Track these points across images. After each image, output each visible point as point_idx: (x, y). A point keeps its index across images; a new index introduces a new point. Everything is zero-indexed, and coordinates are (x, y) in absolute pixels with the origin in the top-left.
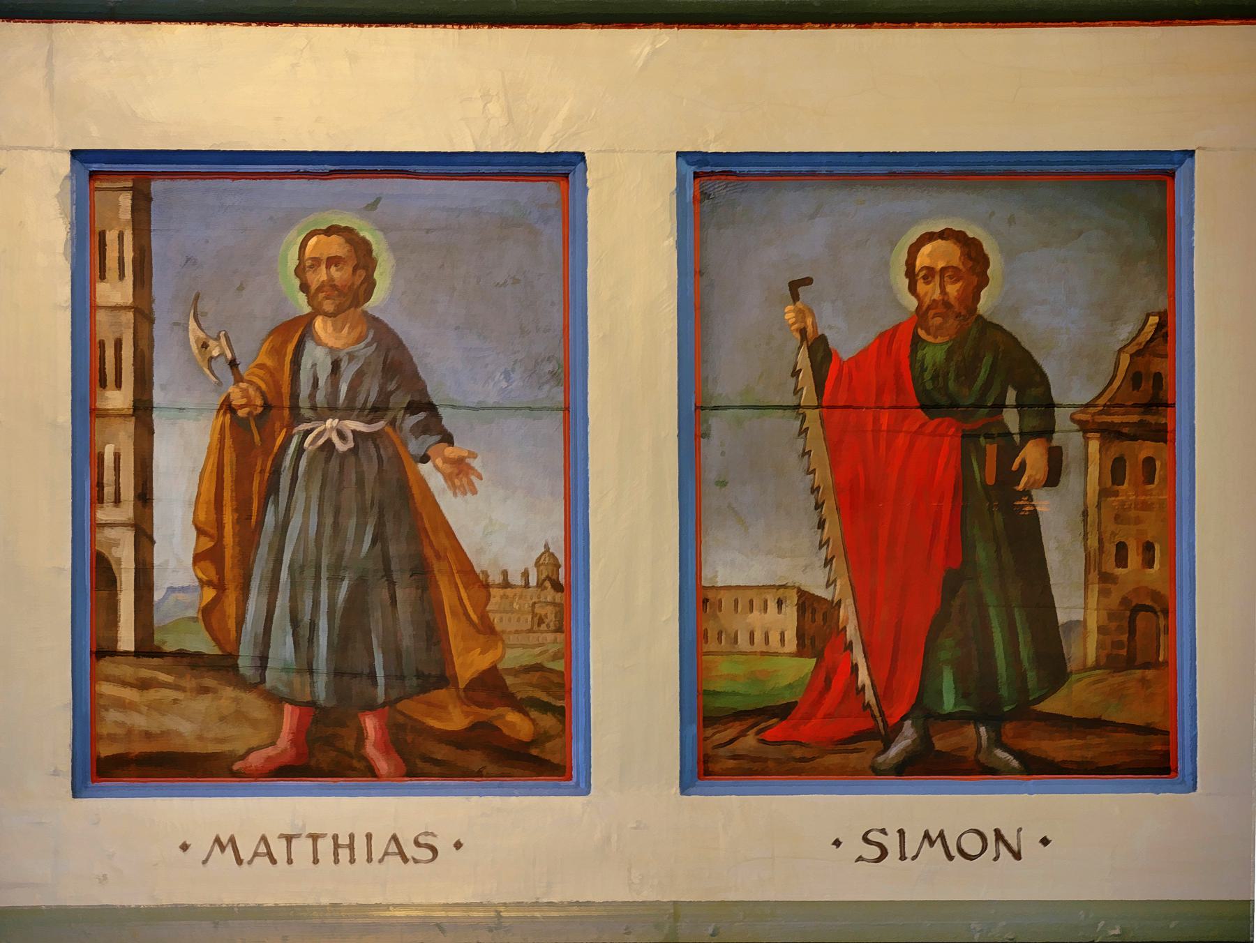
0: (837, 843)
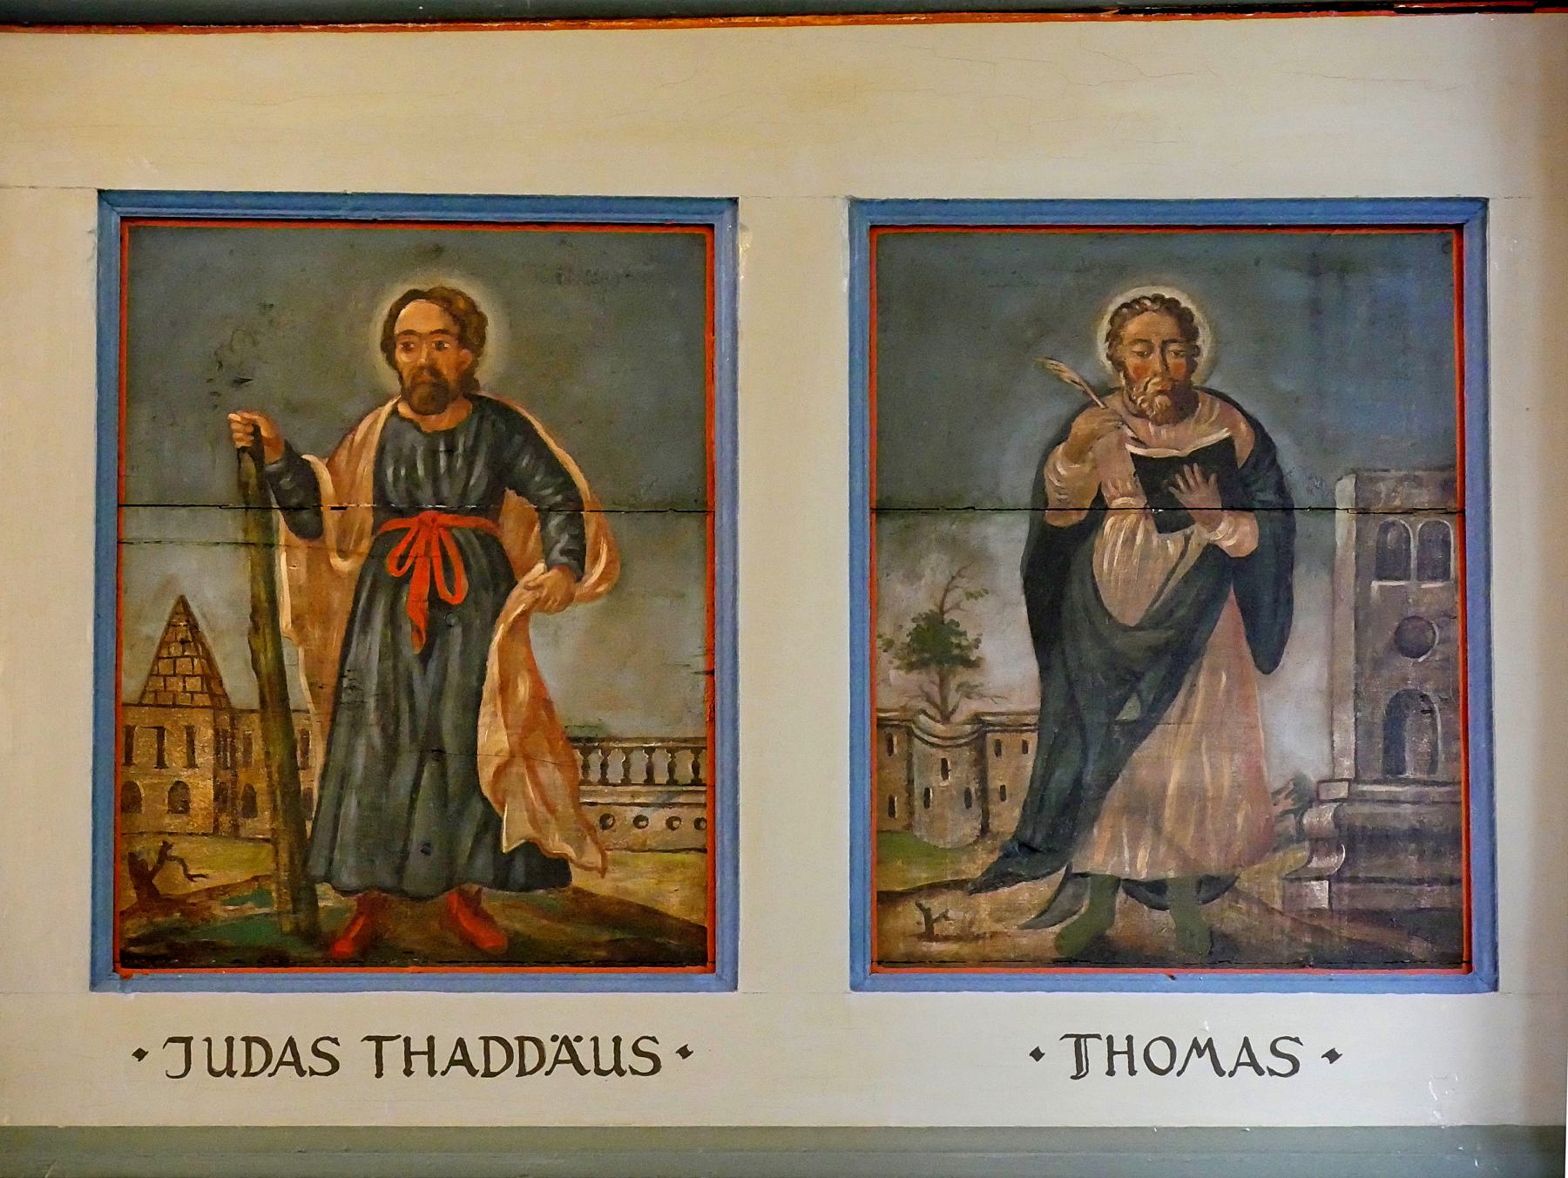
0: (1037, 1054)
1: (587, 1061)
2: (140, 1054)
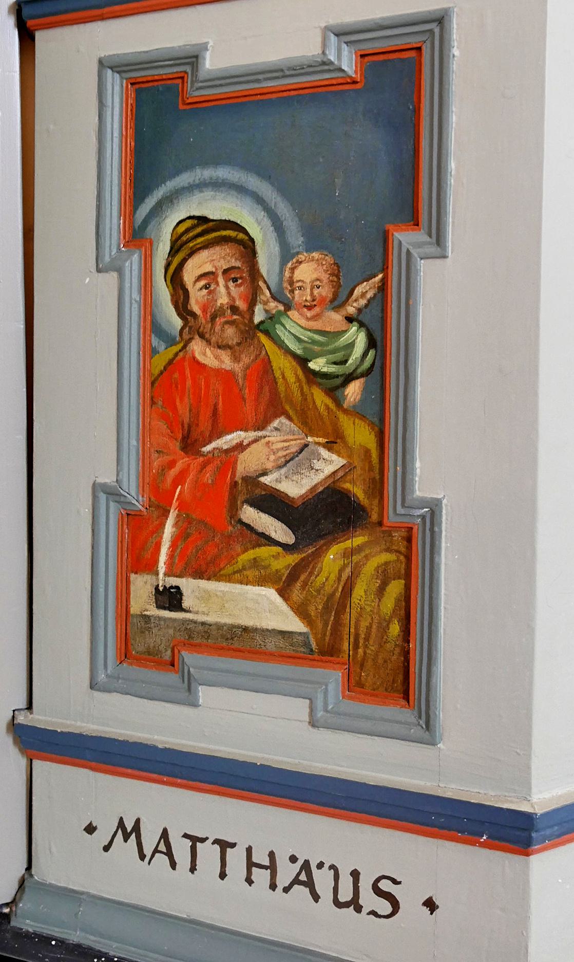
1: (326, 893)
2: (430, 905)
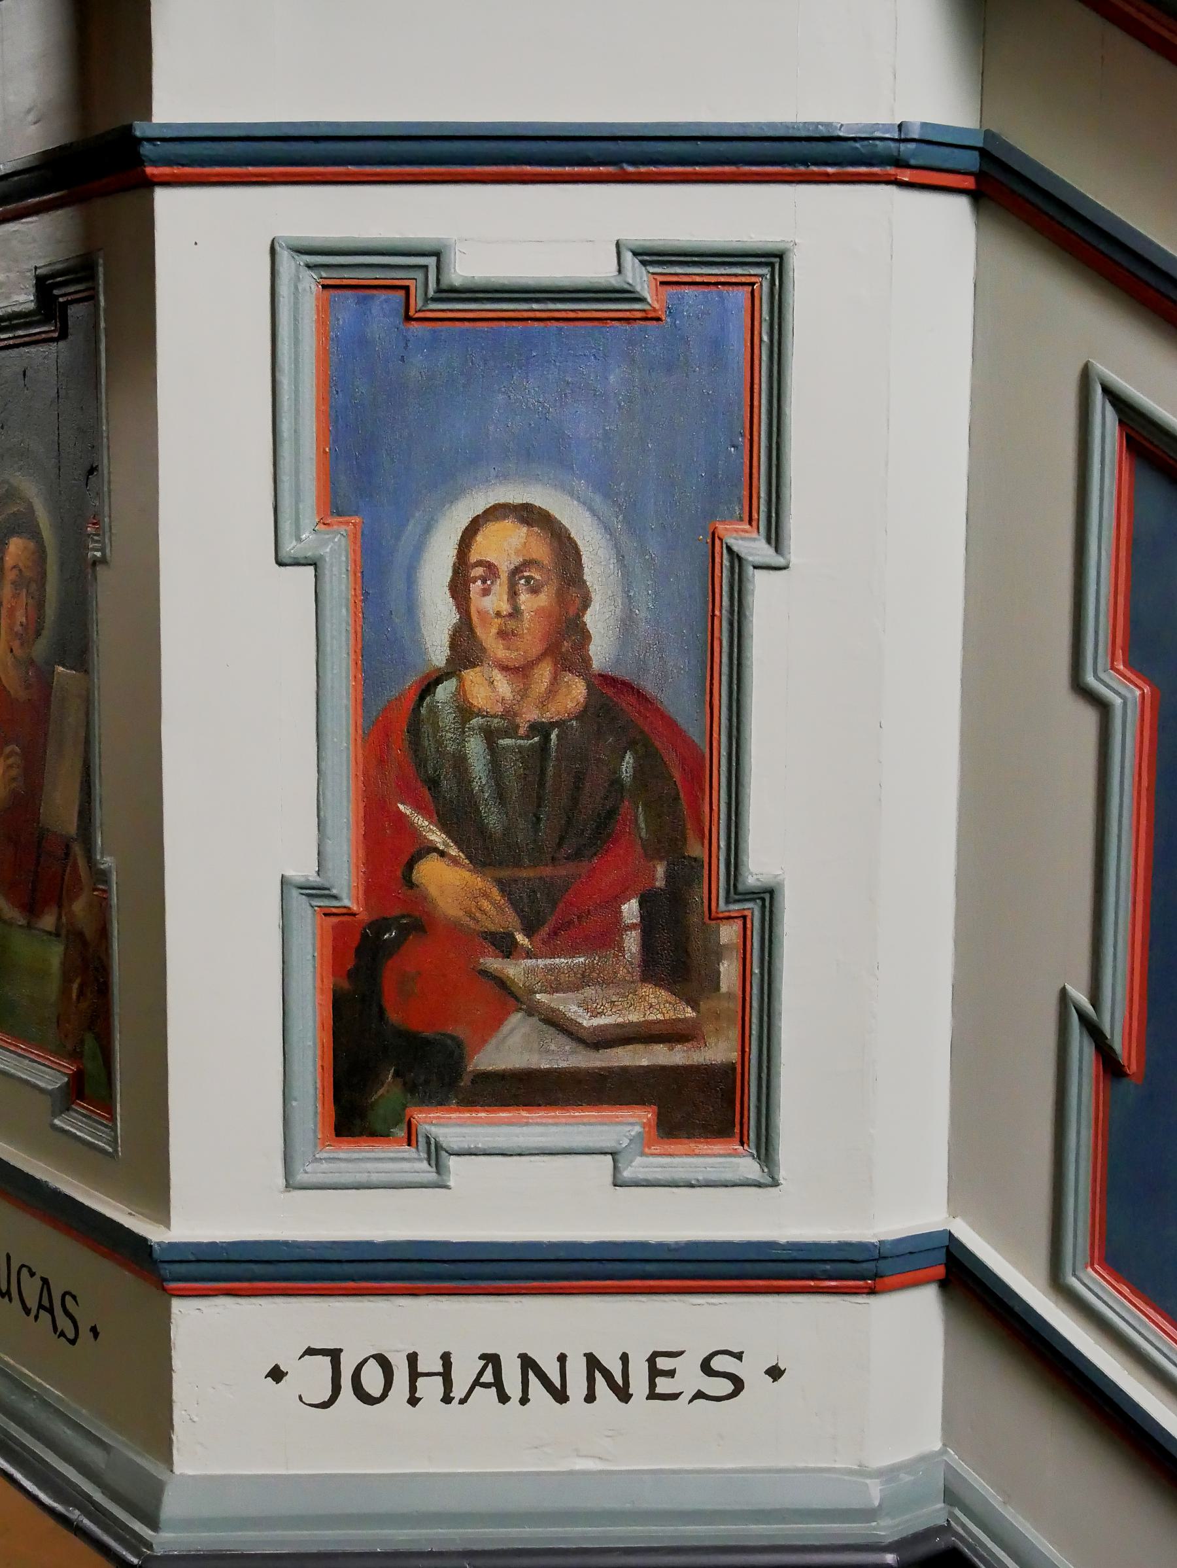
2: (277, 1374)
